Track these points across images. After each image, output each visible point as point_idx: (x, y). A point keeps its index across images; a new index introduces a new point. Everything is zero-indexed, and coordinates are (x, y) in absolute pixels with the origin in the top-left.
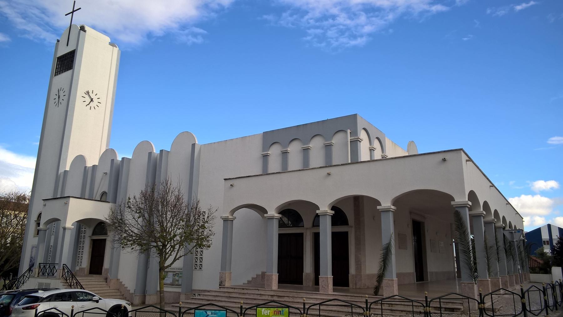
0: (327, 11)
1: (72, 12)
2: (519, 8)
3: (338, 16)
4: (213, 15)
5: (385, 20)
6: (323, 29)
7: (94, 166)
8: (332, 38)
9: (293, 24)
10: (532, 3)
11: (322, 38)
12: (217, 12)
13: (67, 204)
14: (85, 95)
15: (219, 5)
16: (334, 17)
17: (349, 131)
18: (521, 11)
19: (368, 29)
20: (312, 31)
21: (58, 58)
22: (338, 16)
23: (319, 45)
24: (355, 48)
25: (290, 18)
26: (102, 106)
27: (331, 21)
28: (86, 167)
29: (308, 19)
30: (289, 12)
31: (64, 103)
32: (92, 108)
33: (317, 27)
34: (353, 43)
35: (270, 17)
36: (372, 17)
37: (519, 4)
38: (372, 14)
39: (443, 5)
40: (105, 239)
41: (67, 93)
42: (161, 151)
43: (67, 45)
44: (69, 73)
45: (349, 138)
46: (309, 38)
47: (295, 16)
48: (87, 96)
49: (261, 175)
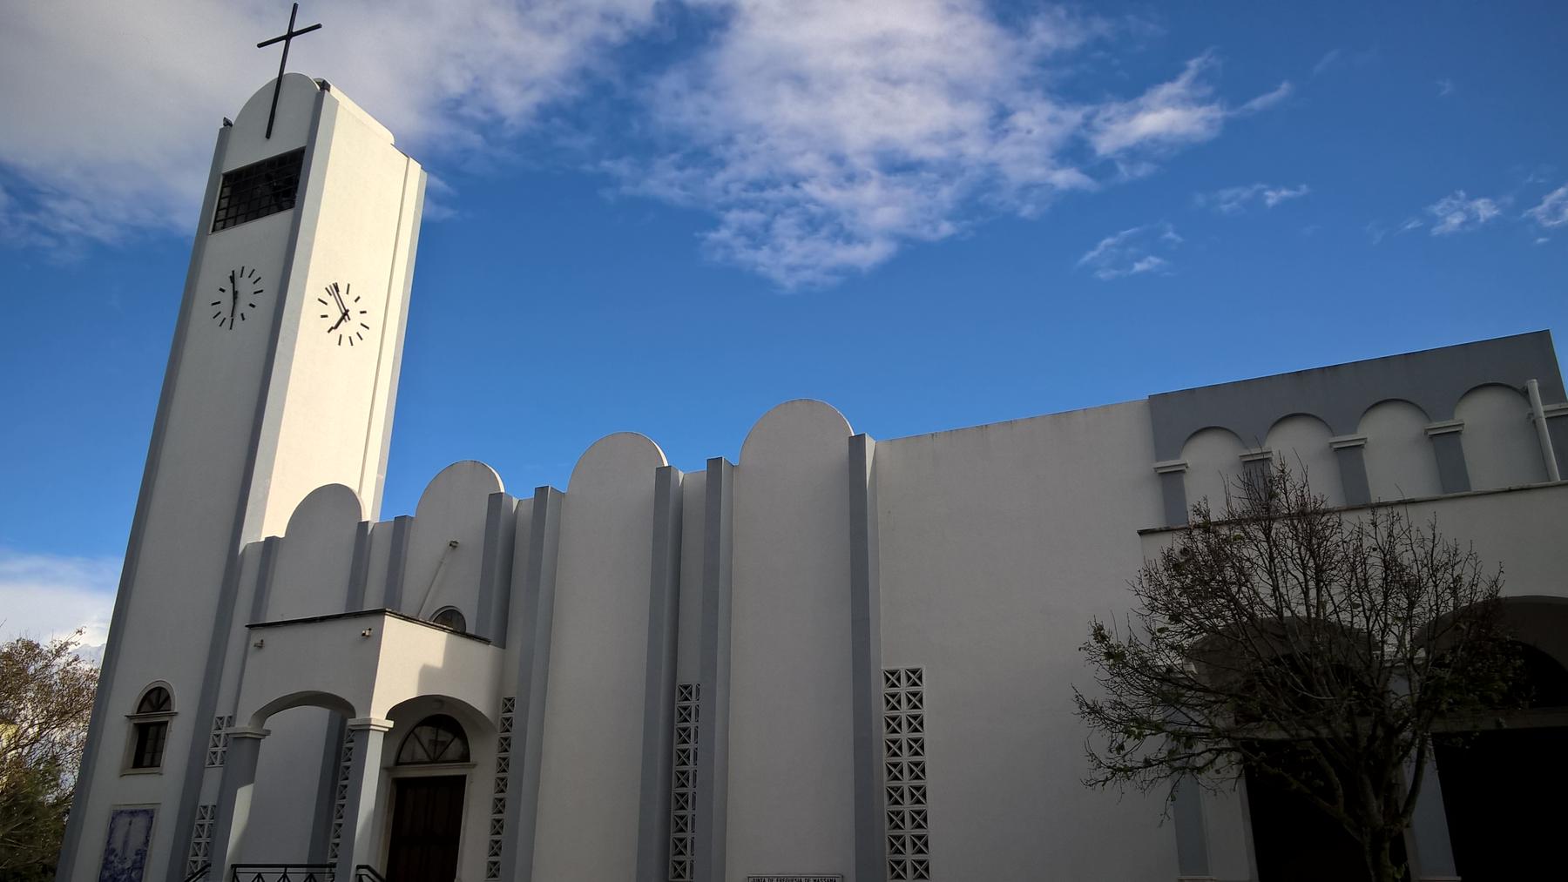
1: (288, 38)
2: (1272, 198)
4: (474, 140)
6: (762, 211)
7: (271, 541)
9: (684, 187)
10: (1304, 189)
12: (483, 129)
13: (372, 642)
14: (326, 297)
15: (488, 110)
20: (734, 216)
21: (228, 177)
25: (674, 174)
26: (372, 337)
27: (787, 190)
28: (496, 499)
30: (674, 157)
31: (257, 320)
32: (345, 341)
33: (747, 206)
37: (1275, 187)
39: (1085, 172)
41: (269, 285)
42: (541, 492)
43: (268, 136)
44: (280, 220)
46: (724, 234)
47: (689, 172)
48: (331, 300)
49: (1161, 531)
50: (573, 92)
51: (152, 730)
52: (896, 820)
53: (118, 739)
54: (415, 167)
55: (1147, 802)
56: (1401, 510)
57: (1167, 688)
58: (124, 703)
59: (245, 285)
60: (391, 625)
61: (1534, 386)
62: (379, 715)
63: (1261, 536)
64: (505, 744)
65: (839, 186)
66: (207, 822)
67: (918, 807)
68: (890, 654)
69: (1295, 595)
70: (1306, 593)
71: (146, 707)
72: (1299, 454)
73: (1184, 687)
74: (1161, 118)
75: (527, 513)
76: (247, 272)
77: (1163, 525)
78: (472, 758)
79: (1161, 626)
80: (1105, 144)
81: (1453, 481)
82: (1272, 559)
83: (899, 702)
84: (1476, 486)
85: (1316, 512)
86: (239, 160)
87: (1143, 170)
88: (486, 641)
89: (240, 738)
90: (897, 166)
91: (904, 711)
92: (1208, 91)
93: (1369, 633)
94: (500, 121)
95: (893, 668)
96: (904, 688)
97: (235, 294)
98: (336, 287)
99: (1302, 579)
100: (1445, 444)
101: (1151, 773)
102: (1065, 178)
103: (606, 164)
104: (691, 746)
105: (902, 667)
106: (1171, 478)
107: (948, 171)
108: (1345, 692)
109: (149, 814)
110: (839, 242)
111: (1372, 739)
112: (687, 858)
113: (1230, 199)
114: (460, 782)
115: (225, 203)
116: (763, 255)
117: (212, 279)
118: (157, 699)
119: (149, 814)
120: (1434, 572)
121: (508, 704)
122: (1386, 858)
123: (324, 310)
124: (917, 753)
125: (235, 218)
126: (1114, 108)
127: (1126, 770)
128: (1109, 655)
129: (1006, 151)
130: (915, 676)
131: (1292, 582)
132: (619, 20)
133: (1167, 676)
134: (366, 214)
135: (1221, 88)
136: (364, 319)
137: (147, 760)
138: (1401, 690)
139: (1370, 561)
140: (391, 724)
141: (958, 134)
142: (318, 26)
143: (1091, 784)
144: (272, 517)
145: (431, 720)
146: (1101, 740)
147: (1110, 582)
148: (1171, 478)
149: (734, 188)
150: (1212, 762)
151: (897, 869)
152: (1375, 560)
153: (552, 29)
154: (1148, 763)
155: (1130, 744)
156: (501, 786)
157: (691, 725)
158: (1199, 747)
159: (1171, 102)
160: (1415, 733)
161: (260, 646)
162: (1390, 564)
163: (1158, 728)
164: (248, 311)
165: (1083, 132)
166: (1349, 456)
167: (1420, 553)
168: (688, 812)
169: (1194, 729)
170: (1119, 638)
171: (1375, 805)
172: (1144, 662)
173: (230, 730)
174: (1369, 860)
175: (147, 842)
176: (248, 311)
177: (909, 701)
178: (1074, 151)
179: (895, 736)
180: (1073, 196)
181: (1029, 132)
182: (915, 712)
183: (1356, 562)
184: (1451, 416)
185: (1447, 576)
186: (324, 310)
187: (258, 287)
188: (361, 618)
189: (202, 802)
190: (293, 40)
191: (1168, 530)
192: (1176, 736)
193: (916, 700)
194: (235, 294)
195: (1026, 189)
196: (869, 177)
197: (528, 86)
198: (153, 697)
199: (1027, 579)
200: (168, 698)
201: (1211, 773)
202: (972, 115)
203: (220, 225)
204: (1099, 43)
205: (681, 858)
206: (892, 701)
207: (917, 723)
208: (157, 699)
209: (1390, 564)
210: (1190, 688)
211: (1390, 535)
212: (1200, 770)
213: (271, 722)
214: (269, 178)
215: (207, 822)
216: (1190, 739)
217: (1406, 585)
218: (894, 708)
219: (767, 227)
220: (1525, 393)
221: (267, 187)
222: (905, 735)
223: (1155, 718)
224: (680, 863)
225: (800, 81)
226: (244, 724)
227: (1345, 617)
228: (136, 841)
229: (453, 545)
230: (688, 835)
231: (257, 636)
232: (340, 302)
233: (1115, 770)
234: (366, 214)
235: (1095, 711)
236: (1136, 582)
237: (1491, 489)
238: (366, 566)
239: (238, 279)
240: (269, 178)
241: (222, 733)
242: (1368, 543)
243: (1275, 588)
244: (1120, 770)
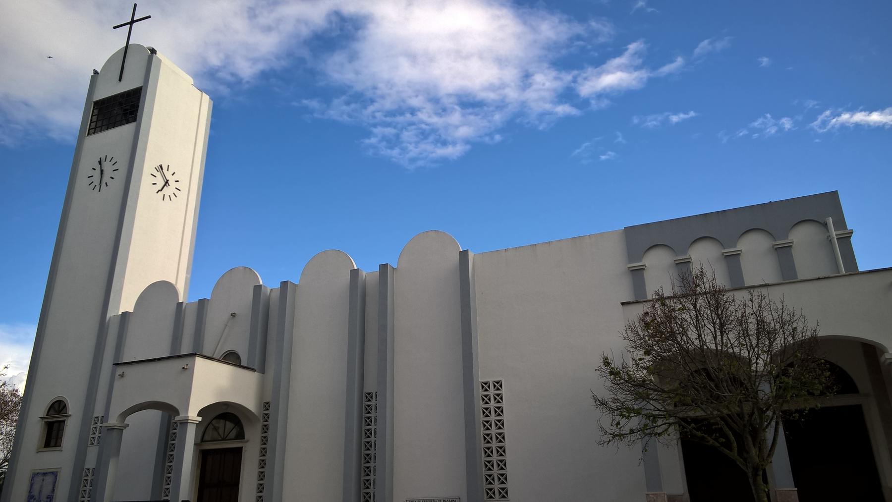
0: (403, 101)
2: (675, 119)
3: (419, 110)
5: (489, 121)
6: (395, 128)
7: (125, 314)
8: (410, 143)
9: (350, 116)
11: (394, 142)
12: (230, 85)
13: (188, 371)
14: (155, 173)
15: (233, 75)
16: (413, 111)
17: (830, 221)
18: (677, 123)
19: (464, 131)
20: (378, 130)
21: (96, 103)
22: (419, 110)
23: (389, 151)
24: (444, 160)
25: (345, 107)
27: (408, 116)
28: (258, 288)
29: (373, 112)
30: (344, 98)
32: (167, 198)
33: (388, 125)
34: (442, 152)
35: (314, 104)
36: (471, 114)
38: (470, 110)
39: (573, 106)
40: (241, 448)
41: (123, 167)
42: (284, 284)
43: (120, 80)
44: (126, 130)
45: (834, 233)
46: (373, 140)
47: (353, 106)
48: (158, 174)
49: (633, 303)
50: (283, 63)
51: (56, 425)
52: (489, 466)
53: (35, 430)
54: (206, 98)
55: (629, 453)
56: (764, 291)
57: (639, 388)
58: (39, 410)
59: (107, 166)
60: (199, 362)
61: (830, 221)
62: (193, 414)
63: (691, 307)
64: (265, 429)
65: (437, 114)
66: (89, 478)
67: (501, 458)
68: (483, 374)
69: (708, 338)
70: (715, 338)
71: (52, 412)
72: (704, 258)
73: (652, 389)
74: (613, 78)
75: (276, 296)
76: (108, 159)
77: (634, 300)
78: (247, 436)
79: (639, 357)
80: (586, 89)
81: (788, 274)
82: (697, 320)
83: (489, 399)
84: (800, 277)
85: (720, 291)
86: (103, 93)
87: (605, 103)
88: (253, 370)
89: (111, 429)
90: (469, 103)
91: (492, 404)
92: (639, 61)
93: (750, 359)
94: (239, 81)
95: (485, 380)
96: (492, 392)
97: (102, 171)
98: (161, 166)
99: (713, 330)
100: (783, 252)
101: (633, 437)
102: (563, 109)
103: (305, 102)
104: (372, 427)
105: (491, 380)
106: (637, 273)
107: (501, 105)
108: (739, 391)
109: (55, 474)
110: (439, 145)
111: (751, 415)
112: (371, 490)
113: (652, 122)
114: (240, 450)
115: (95, 118)
116: (396, 152)
117: (88, 163)
118: (58, 407)
119: (55, 474)
120: (783, 325)
121: (267, 406)
122: (760, 479)
123: (154, 180)
124: (500, 428)
125: (101, 127)
126: (590, 70)
127: (620, 435)
128: (611, 373)
129: (531, 95)
130: (498, 385)
131: (707, 331)
132: (306, 23)
133: (643, 384)
134: (177, 126)
135: (650, 60)
136: (177, 185)
137: (53, 443)
138: (766, 389)
139: (749, 321)
140: (200, 419)
141: (503, 86)
142: (149, 17)
143: (601, 443)
144: (126, 301)
145: (223, 416)
146: (607, 419)
147: (608, 333)
148: (637, 273)
149: (378, 115)
150: (666, 430)
151: (490, 494)
152: (752, 319)
153: (268, 29)
154: (632, 432)
155: (623, 421)
156: (263, 452)
157: (373, 415)
158: (660, 422)
159: (620, 68)
160: (774, 413)
161: (122, 376)
162: (760, 322)
163: (638, 412)
164: (109, 181)
165: (573, 85)
166: (732, 260)
167: (775, 315)
168: (372, 465)
169: (657, 412)
170: (617, 364)
171: (754, 451)
172: (630, 377)
173: (104, 425)
174: (751, 481)
175: (53, 490)
176: (109, 181)
177: (495, 399)
178: (568, 95)
179: (487, 419)
180: (567, 119)
181: (544, 85)
182: (499, 405)
183: (742, 321)
184: (787, 237)
185: (790, 328)
186: (154, 180)
187: (115, 167)
188: (181, 357)
189: (86, 467)
190: (135, 25)
191: (637, 302)
192: (647, 416)
193: (499, 398)
194: (102, 171)
195: (542, 115)
196: (454, 109)
197: (255, 61)
198: (56, 406)
199: (562, 333)
200: (65, 406)
201: (666, 436)
202: (510, 75)
203: (92, 131)
204: (578, 37)
205: (368, 491)
206: (486, 399)
207: (499, 411)
208: (58, 407)
209: (760, 322)
210: (655, 390)
211: (760, 306)
212: (659, 434)
213: (129, 419)
214: (121, 104)
215: (89, 478)
216: (655, 417)
217: (768, 333)
218: (487, 403)
219: (397, 136)
220: (825, 225)
221: (119, 108)
222: (493, 418)
223: (636, 407)
224: (367, 493)
225: (413, 57)
226: (113, 421)
227: (736, 350)
228: (47, 491)
229: (233, 315)
230: (372, 477)
231: (120, 370)
232: (164, 176)
233: (614, 436)
234: (177, 126)
235: (603, 403)
236: (624, 332)
237: (809, 278)
238: (186, 332)
239: (103, 163)
240: (121, 104)
241: (98, 426)
242: (748, 311)
243: (700, 336)
244: (617, 435)
